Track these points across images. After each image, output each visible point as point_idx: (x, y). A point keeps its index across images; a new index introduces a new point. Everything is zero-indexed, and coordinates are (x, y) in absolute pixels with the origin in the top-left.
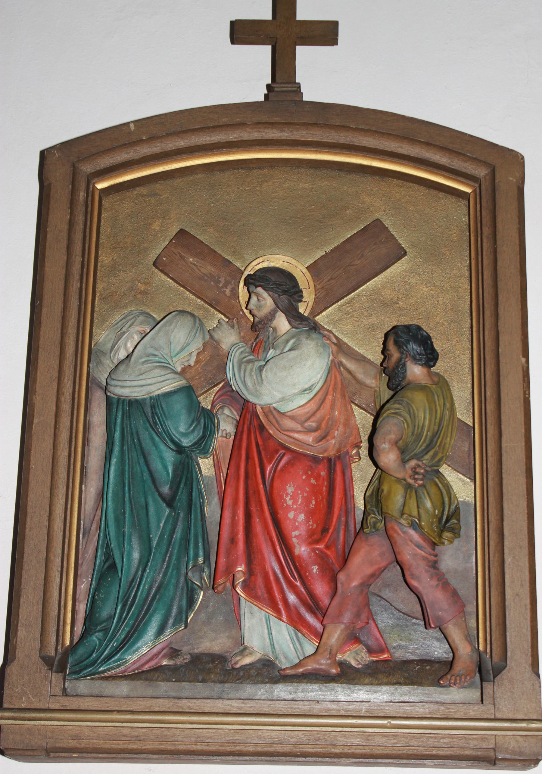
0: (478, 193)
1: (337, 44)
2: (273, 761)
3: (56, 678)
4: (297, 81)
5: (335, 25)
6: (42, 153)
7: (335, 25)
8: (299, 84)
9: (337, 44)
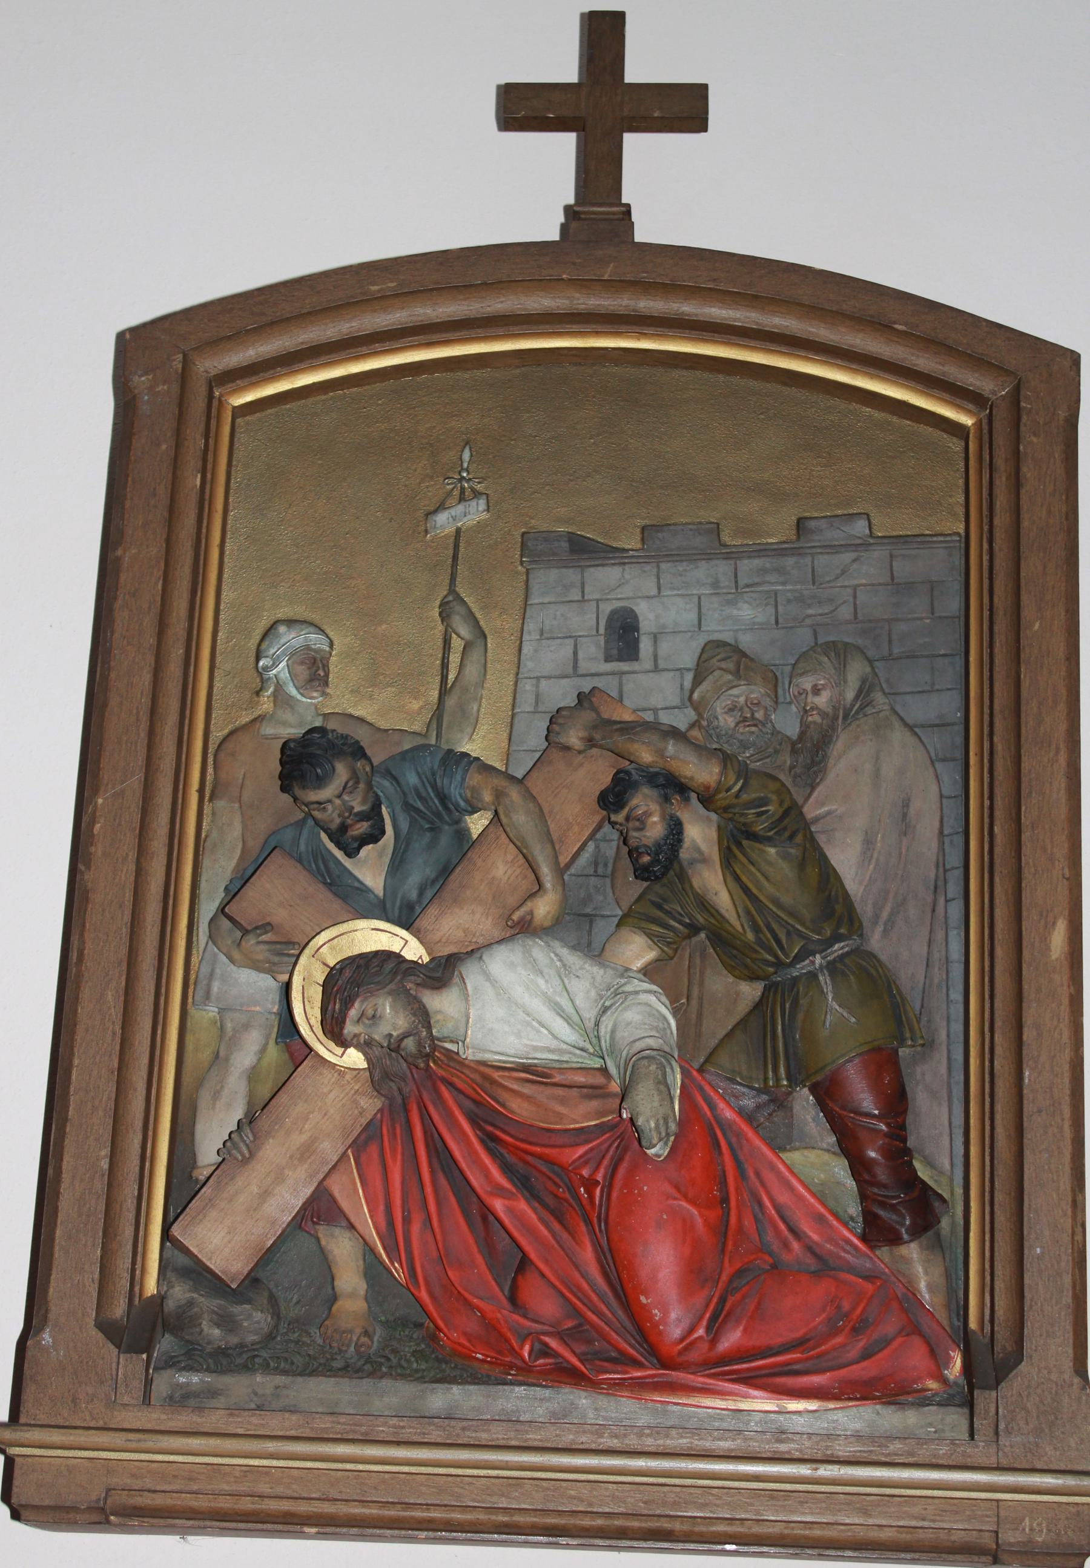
0: (987, 427)
1: (706, 130)
2: (288, 1531)
3: (132, 1366)
4: (624, 201)
5: (701, 91)
6: (120, 336)
7: (701, 91)
8: (628, 206)
9: (706, 130)
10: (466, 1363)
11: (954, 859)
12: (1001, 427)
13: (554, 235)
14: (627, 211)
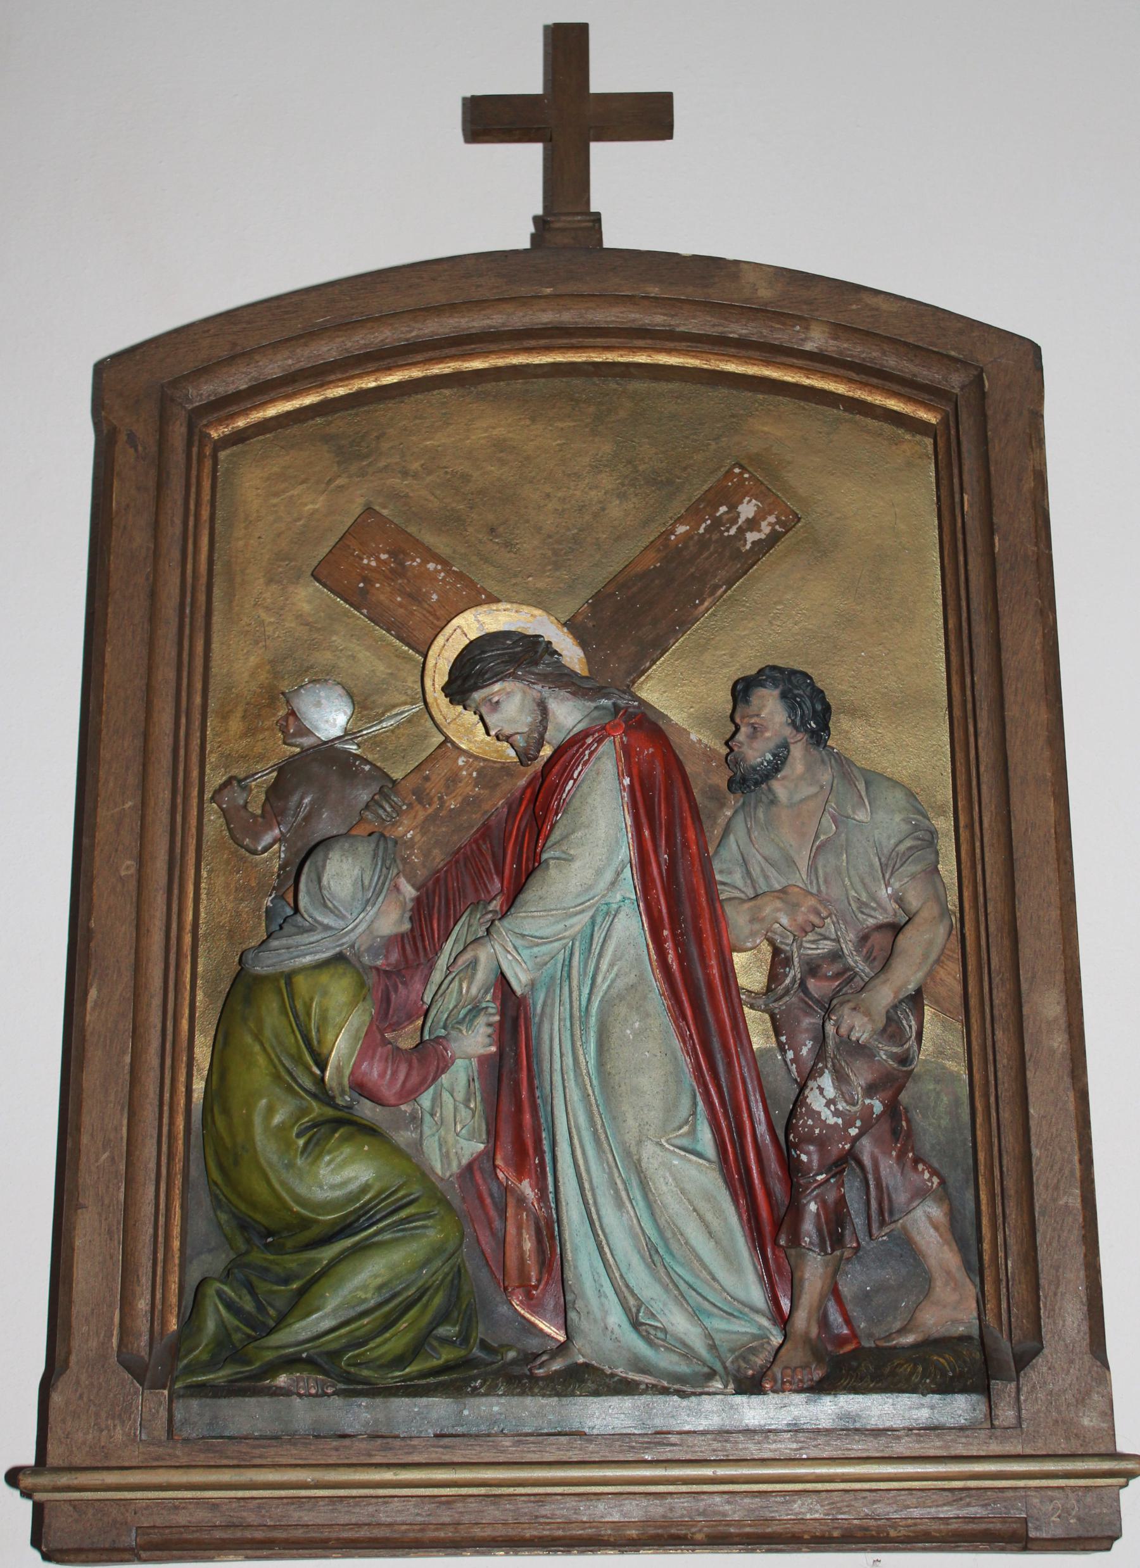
0: (952, 420)
1: (670, 137)
4: (593, 209)
5: (665, 100)
6: (100, 369)
7: (665, 100)
8: (599, 214)
9: (670, 137)
10: (271, 1257)
11: (593, 1451)
12: (967, 423)
13: (527, 245)
14: (597, 218)
